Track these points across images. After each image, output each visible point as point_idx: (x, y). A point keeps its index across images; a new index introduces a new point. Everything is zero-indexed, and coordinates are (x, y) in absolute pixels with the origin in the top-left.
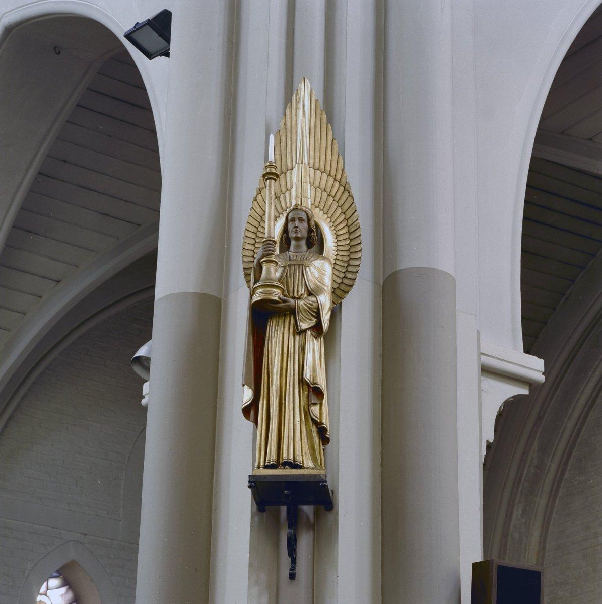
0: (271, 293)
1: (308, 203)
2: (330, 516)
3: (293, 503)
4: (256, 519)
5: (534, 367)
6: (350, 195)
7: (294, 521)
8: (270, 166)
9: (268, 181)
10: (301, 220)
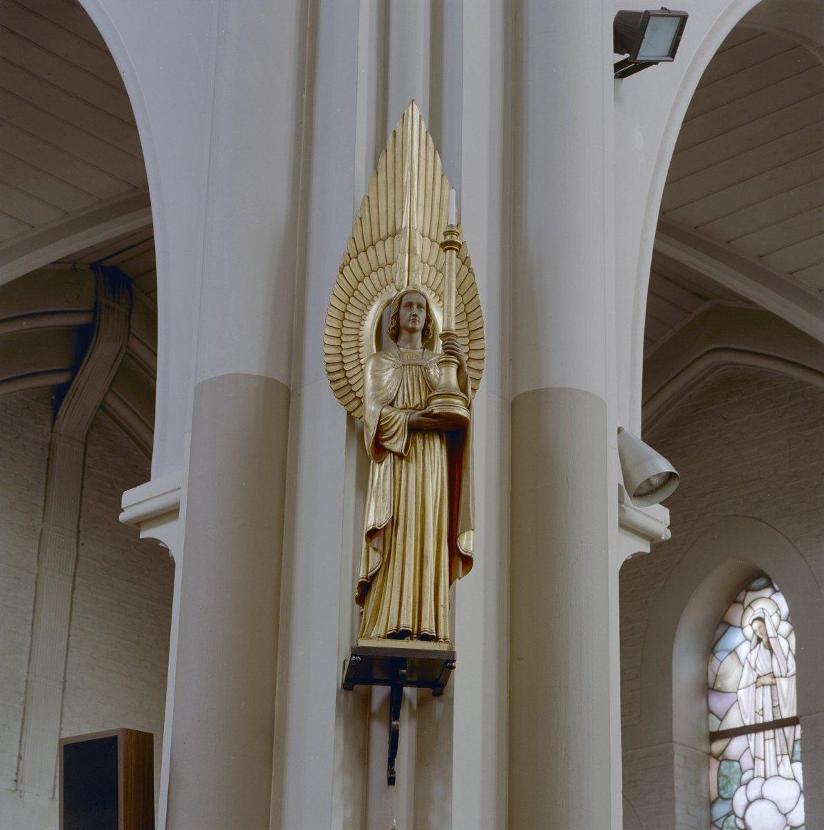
0: (451, 405)
1: (418, 281)
2: (438, 706)
3: (396, 680)
4: (342, 696)
5: (422, 633)
6: (470, 271)
7: (395, 705)
8: (451, 232)
9: (448, 251)
10: (420, 306)
